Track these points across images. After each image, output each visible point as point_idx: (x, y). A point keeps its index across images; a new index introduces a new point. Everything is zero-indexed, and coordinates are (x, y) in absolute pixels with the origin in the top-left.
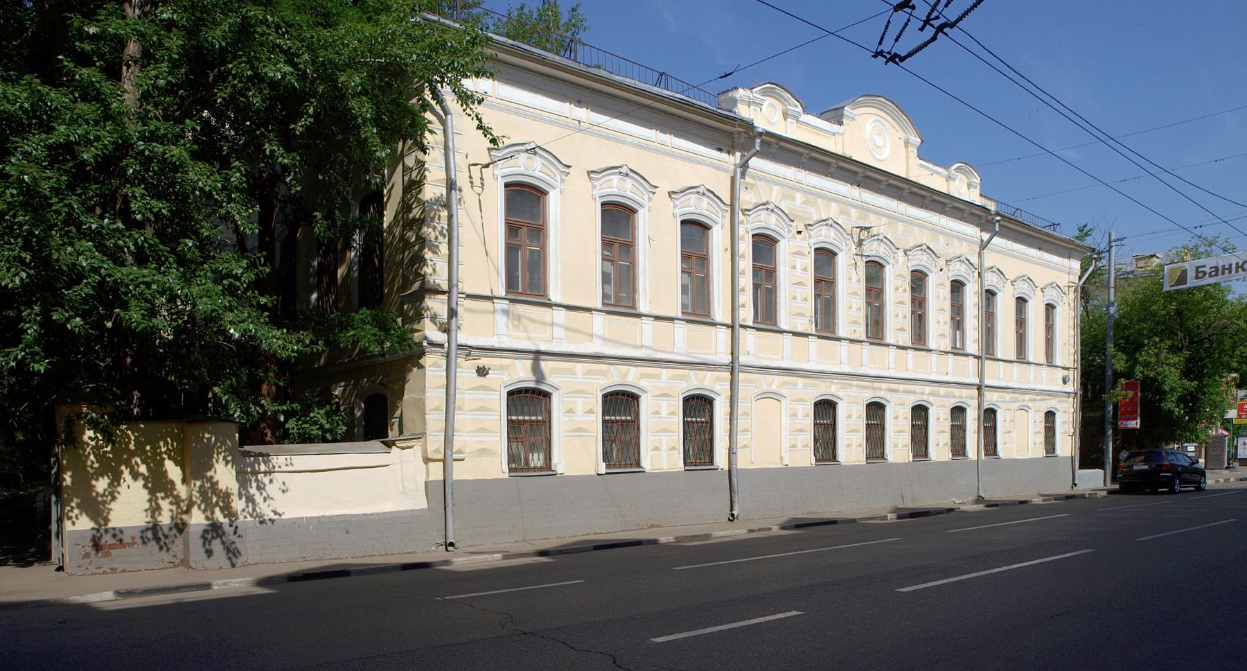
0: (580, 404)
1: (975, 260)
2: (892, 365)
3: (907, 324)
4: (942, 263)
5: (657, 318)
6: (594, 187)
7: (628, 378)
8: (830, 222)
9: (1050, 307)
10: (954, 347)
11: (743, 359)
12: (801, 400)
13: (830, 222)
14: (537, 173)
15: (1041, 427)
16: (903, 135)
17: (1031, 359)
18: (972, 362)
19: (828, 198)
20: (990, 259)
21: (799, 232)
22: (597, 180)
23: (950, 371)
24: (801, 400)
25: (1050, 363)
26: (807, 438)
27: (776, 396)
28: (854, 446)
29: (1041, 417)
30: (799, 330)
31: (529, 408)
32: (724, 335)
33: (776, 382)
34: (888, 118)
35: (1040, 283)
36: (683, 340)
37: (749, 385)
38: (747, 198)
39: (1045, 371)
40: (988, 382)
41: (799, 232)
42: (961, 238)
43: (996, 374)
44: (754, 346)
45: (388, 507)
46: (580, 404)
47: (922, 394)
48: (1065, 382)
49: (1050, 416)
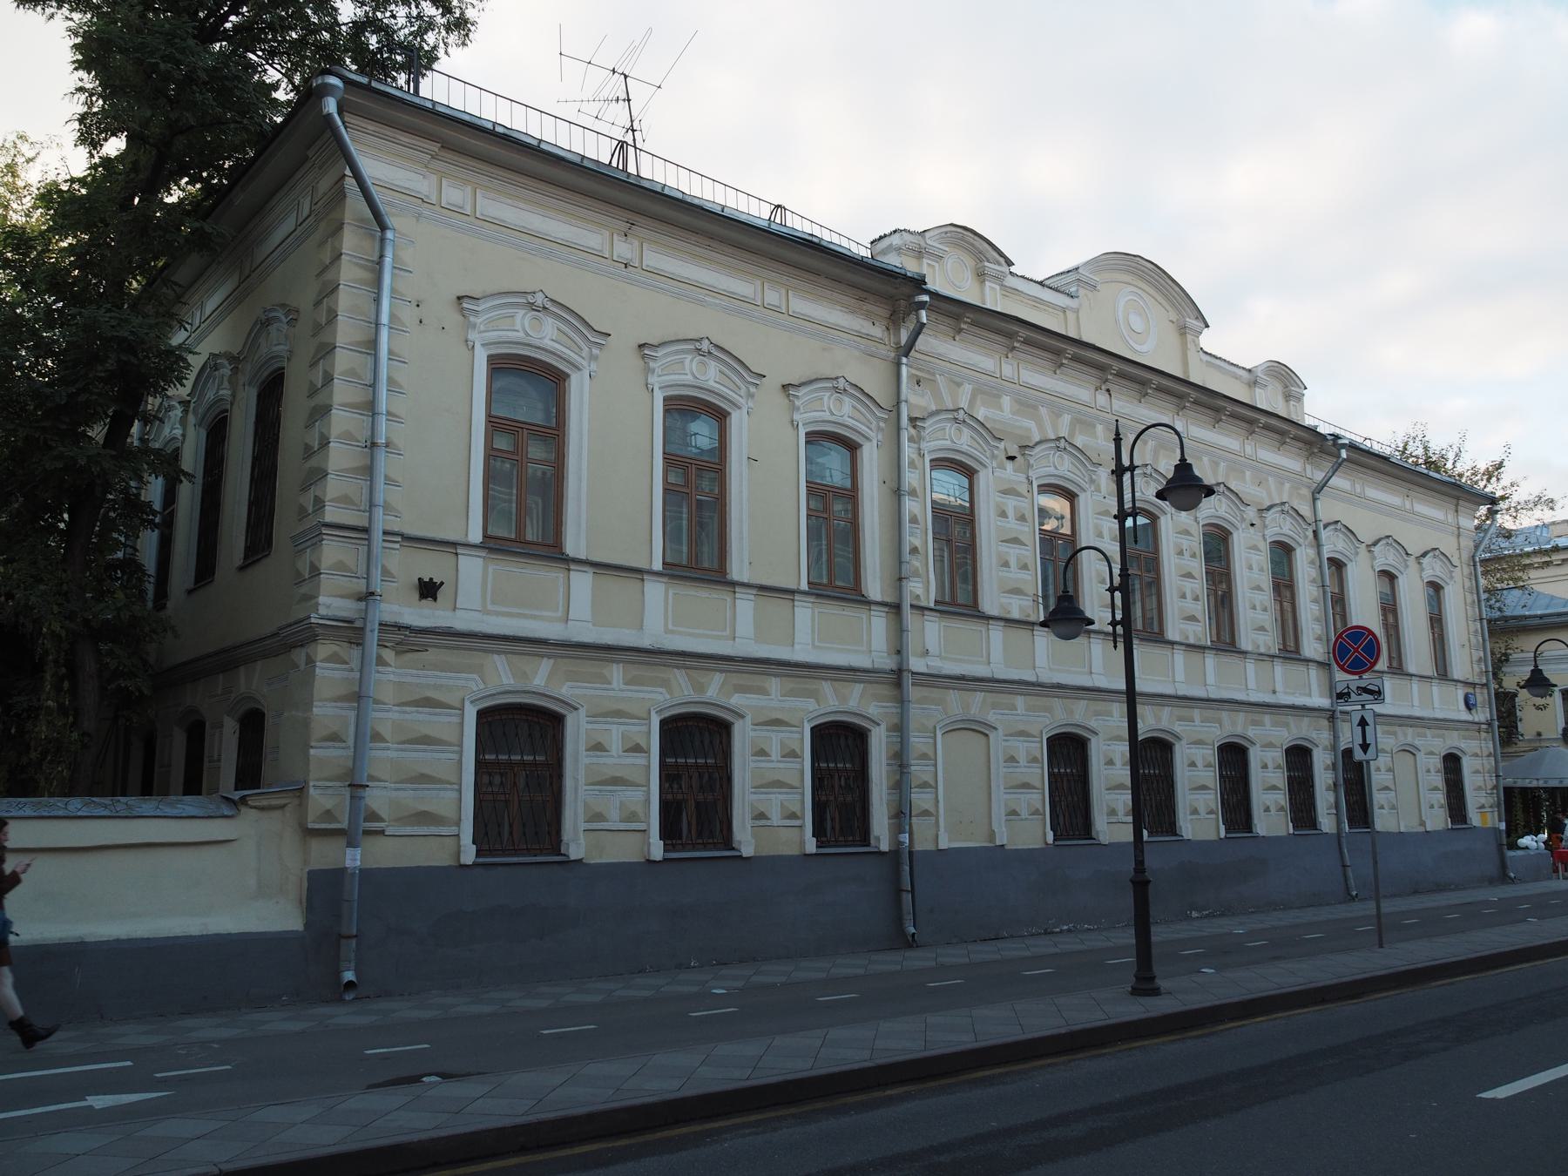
0: (1022, 749)
1: (1305, 510)
2: (1416, 703)
3: (1200, 609)
4: (1251, 513)
5: (762, 588)
6: (794, 409)
7: (714, 692)
8: (1286, 508)
9: (1436, 588)
10: (1284, 649)
11: (1140, 686)
12: (1022, 733)
13: (1286, 508)
14: (547, 343)
15: (1438, 780)
16: (1173, 316)
17: (1412, 669)
18: (1314, 673)
19: (1058, 405)
20: (1328, 509)
21: (1012, 458)
22: (654, 358)
23: (1279, 688)
24: (1022, 733)
25: (1442, 672)
26: (1038, 799)
27: (981, 729)
28: (1273, 811)
29: (1436, 763)
30: (1016, 615)
31: (522, 745)
32: (879, 624)
33: (977, 704)
34: (1152, 291)
35: (1366, 536)
36: (810, 632)
37: (926, 711)
38: (915, 400)
39: (1436, 689)
40: (916, 664)
41: (1012, 458)
42: (1281, 474)
43: (1159, 672)
44: (937, 644)
45: (254, 930)
46: (775, 740)
47: (1233, 726)
48: (1469, 706)
49: (1452, 763)
